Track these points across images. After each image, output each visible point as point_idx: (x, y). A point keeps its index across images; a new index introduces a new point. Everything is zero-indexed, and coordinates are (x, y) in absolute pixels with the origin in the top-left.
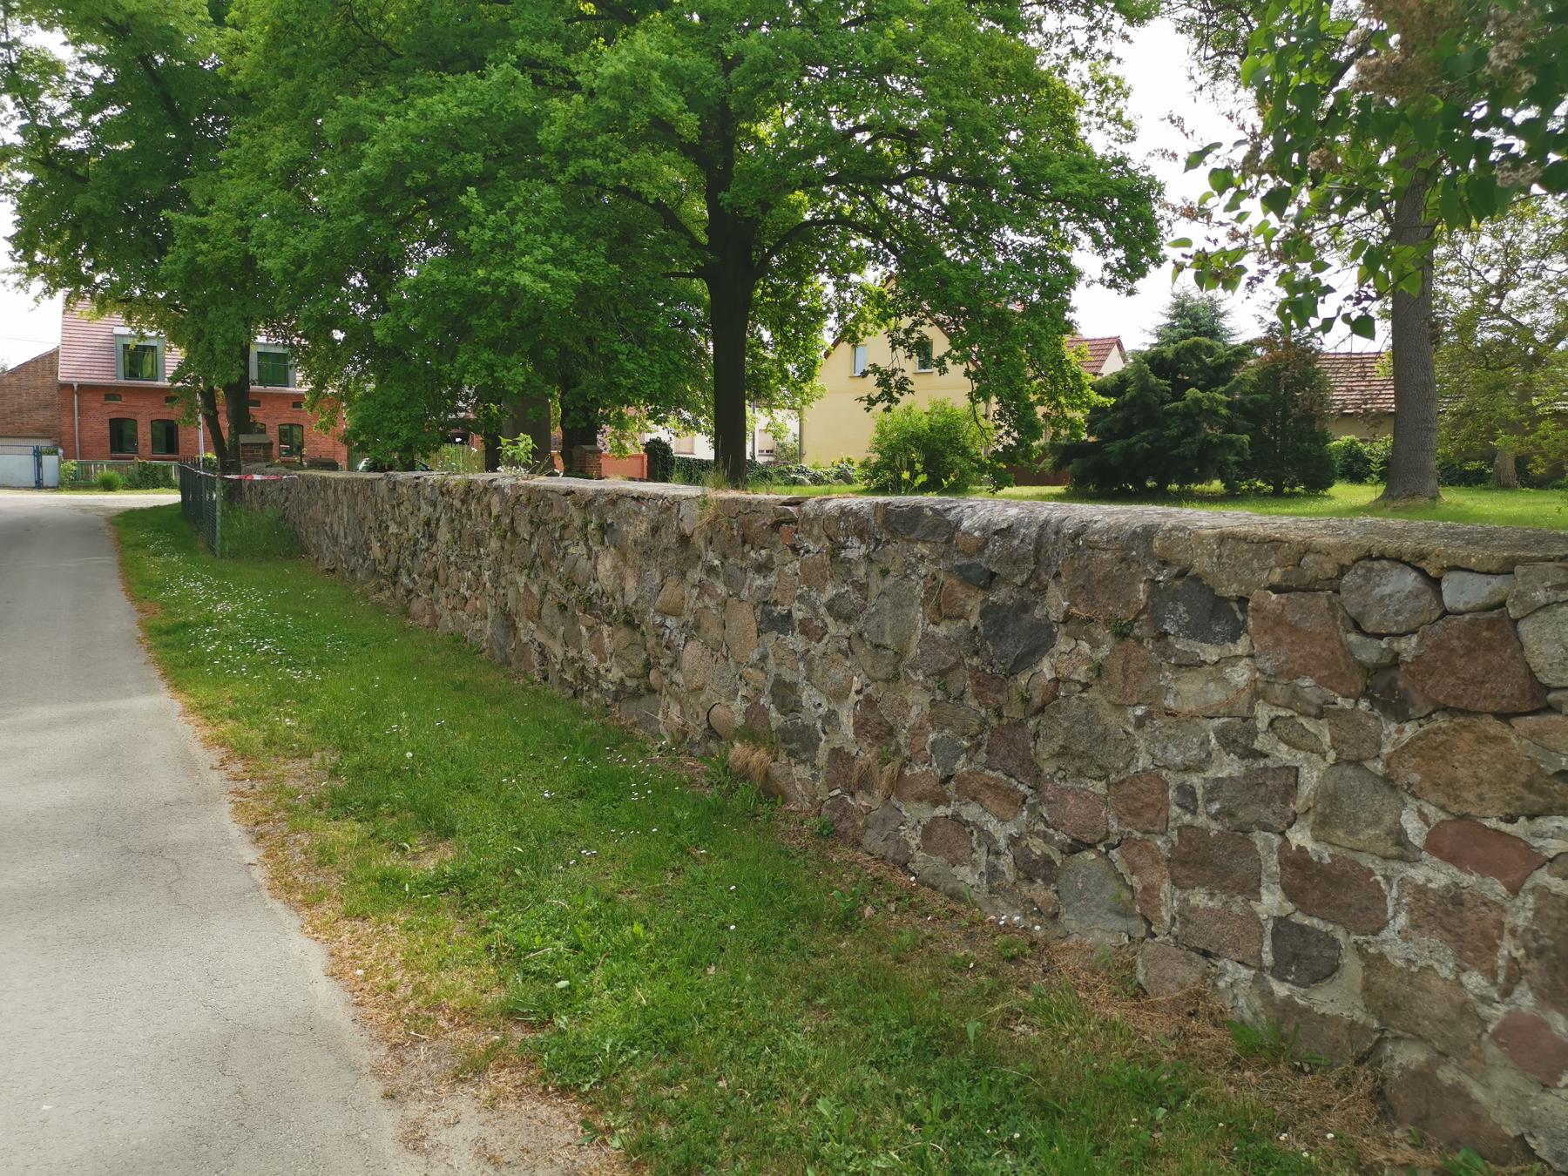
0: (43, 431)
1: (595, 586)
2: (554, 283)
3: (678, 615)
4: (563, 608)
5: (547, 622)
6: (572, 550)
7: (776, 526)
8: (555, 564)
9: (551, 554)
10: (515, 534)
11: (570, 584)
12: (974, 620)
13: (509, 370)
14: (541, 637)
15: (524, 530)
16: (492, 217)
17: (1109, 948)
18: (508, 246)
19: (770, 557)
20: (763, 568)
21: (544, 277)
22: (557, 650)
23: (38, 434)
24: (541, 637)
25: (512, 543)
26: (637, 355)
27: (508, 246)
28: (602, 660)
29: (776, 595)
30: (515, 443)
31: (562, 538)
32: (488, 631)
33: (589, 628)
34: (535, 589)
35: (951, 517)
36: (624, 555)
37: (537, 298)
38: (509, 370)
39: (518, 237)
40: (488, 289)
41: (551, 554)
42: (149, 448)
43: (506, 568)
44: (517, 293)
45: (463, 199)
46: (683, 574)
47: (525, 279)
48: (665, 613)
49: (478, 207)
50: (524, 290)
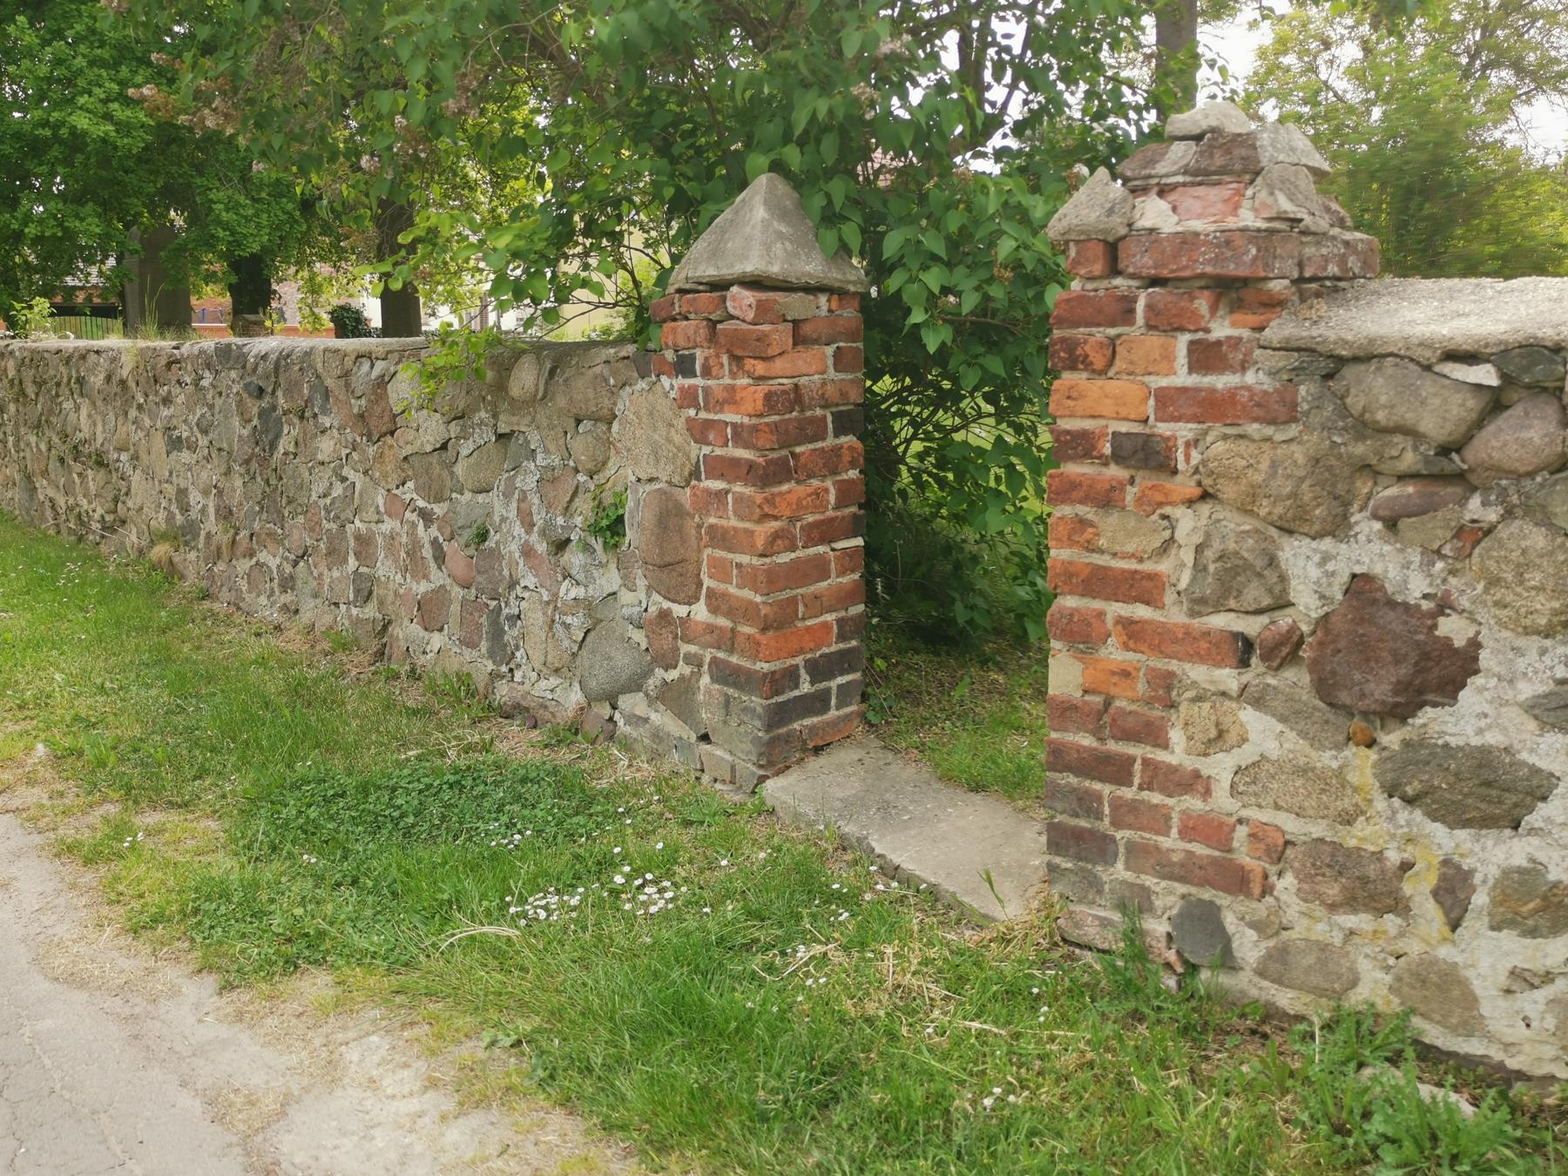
0: (1196, 173)
1: (80, 435)
2: (118, 124)
3: (127, 450)
4: (62, 460)
5: (52, 476)
6: (65, 405)
7: (169, 365)
8: (54, 419)
9: (51, 411)
10: (25, 395)
11: (65, 437)
12: (255, 422)
13: (82, 220)
14: (51, 493)
15: (30, 390)
16: (48, 49)
17: (1345, 963)
18: (69, 82)
19: (169, 392)
20: (167, 401)
21: (108, 117)
22: (61, 501)
23: (1188, 179)
24: (51, 493)
25: (24, 405)
26: (238, 204)
27: (69, 82)
28: (90, 503)
29: (174, 422)
30: (31, 307)
31: (57, 395)
32: (17, 497)
33: (80, 475)
34: (43, 447)
35: (245, 350)
36: (94, 403)
37: (104, 141)
38: (82, 220)
39: (81, 71)
40: (48, 132)
41: (51, 411)
42: (1185, 369)
43: (23, 430)
44: (77, 140)
45: (11, 29)
46: (126, 414)
47: (82, 121)
48: (120, 450)
49: (30, 39)
50: (85, 133)
